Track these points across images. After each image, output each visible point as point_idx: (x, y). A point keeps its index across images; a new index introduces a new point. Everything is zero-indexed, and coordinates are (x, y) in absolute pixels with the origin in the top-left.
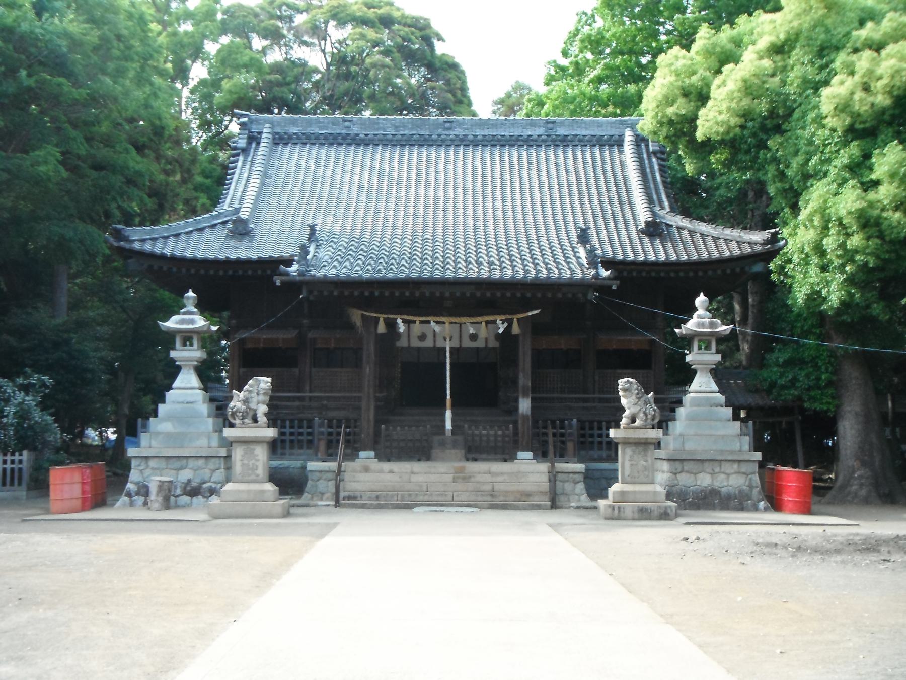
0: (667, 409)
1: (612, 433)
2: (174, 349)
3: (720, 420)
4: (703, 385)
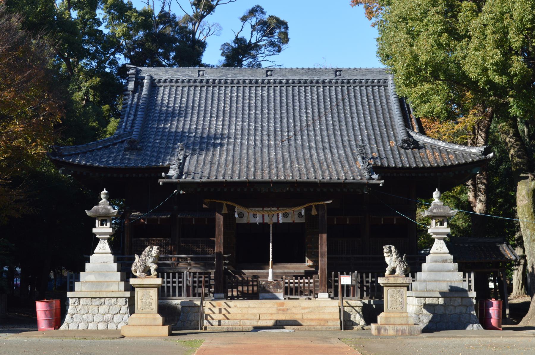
0: (414, 266)
1: (381, 281)
2: (95, 227)
3: (449, 271)
4: (439, 248)
